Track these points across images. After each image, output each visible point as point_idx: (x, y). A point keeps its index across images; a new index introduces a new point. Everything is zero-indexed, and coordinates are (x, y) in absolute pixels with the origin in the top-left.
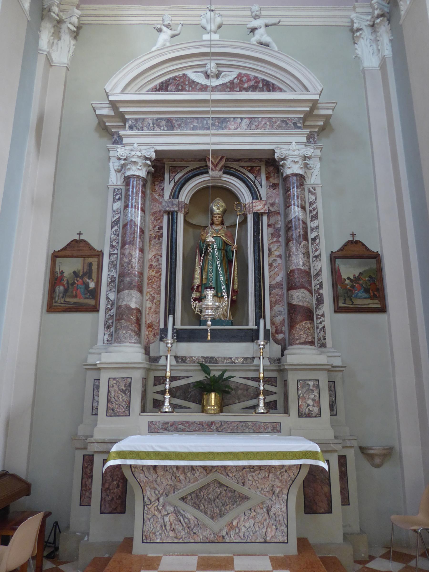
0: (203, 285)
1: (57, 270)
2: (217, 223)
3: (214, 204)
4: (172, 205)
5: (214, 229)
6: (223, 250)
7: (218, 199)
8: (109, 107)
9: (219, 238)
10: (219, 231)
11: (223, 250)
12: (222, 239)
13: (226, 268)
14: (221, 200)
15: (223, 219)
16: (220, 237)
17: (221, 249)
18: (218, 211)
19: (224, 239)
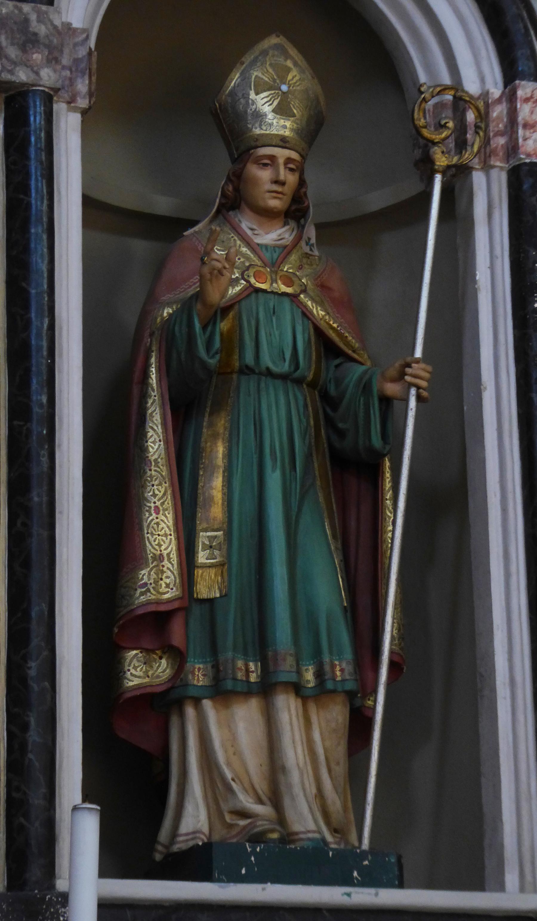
0: (196, 610)
1: (228, 224)
2: (274, 203)
3: (256, 73)
4: (23, 48)
5: (248, 243)
6: (313, 385)
7: (274, 40)
8: (257, 147)
9: (287, 303)
10: (284, 259)
11: (313, 385)
12: (306, 315)
13: (316, 319)
14: (293, 51)
15: (302, 183)
16: (293, 297)
17: (299, 382)
18: (280, 126)
19: (318, 312)
